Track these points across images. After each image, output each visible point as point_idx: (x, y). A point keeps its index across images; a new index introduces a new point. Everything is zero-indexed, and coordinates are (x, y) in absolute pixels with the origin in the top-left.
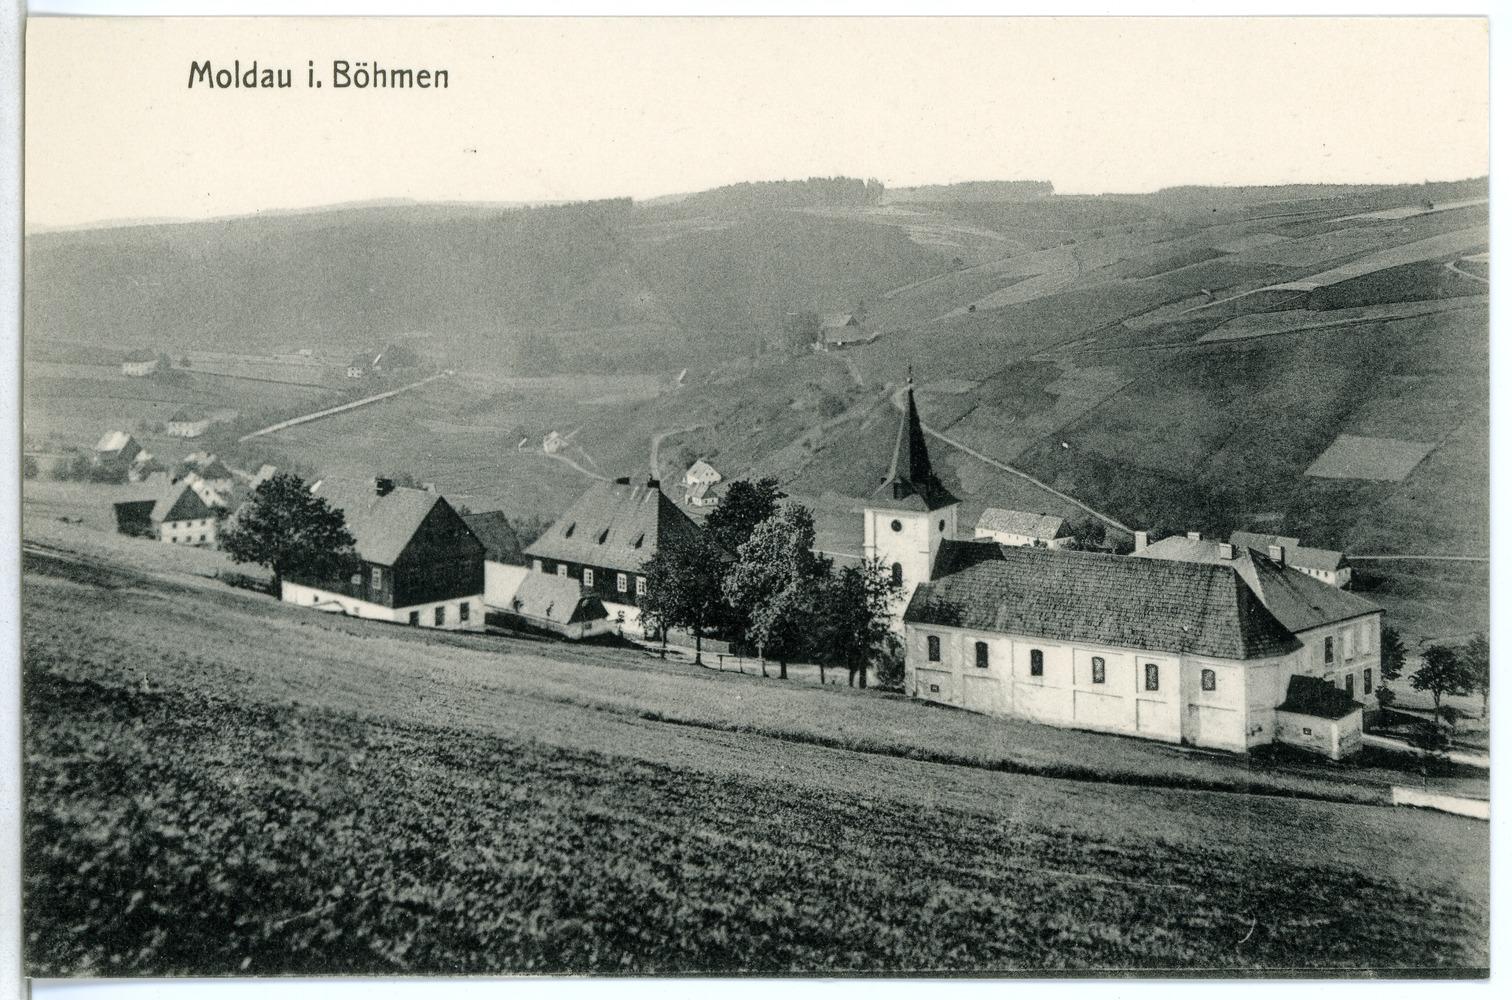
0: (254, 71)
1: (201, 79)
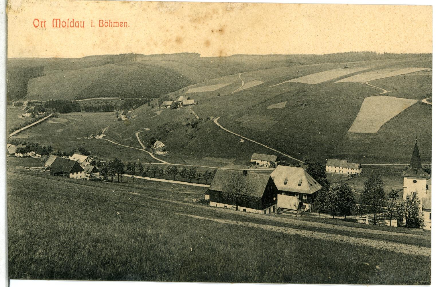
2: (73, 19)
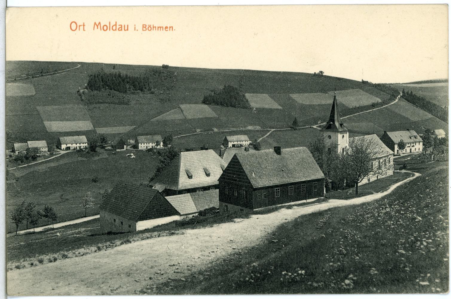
0: (116, 25)
1: (98, 28)
2: (116, 23)
